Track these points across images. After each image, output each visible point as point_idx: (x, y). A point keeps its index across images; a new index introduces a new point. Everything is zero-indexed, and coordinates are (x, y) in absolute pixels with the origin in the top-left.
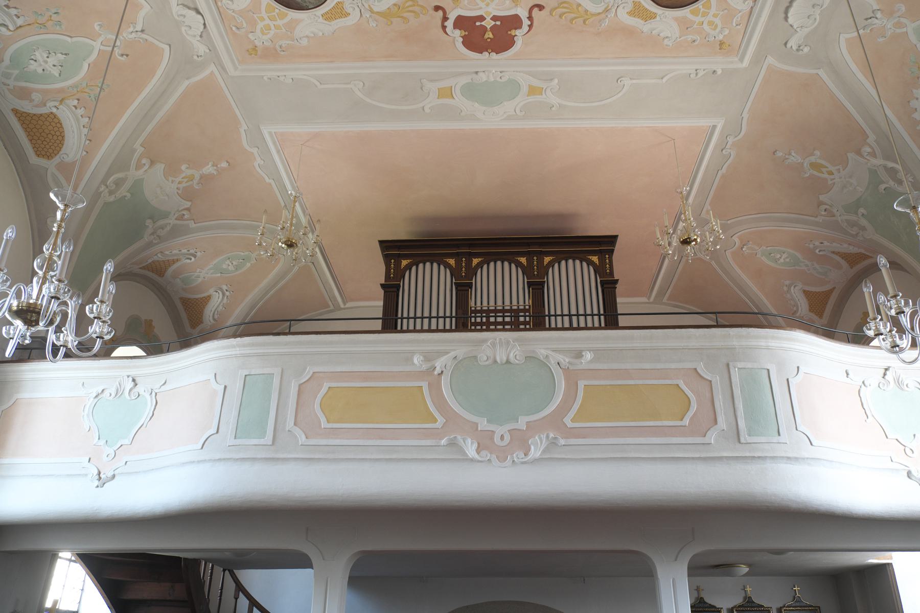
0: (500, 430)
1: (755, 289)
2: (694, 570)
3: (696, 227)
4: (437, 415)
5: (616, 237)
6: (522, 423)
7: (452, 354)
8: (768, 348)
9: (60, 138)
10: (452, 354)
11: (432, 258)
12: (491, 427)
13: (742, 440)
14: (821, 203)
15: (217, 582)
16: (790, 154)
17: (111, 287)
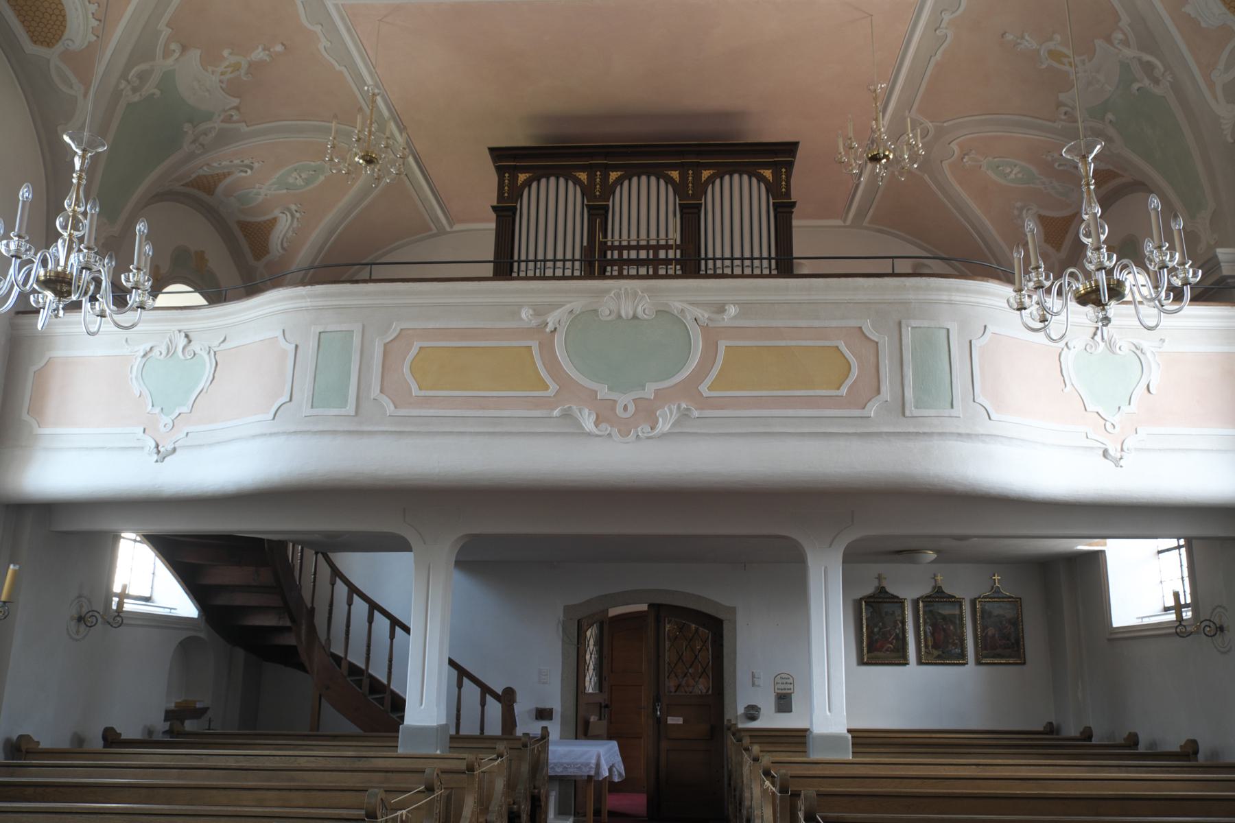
0: (624, 399)
1: (978, 212)
2: (851, 558)
3: (888, 140)
4: (548, 380)
5: (796, 144)
6: (649, 391)
7: (568, 307)
8: (950, 303)
9: (60, 18)
10: (568, 307)
11: (558, 172)
12: (613, 396)
13: (907, 413)
14: (1060, 104)
15: (310, 567)
16: (1023, 38)
17: (147, 248)
